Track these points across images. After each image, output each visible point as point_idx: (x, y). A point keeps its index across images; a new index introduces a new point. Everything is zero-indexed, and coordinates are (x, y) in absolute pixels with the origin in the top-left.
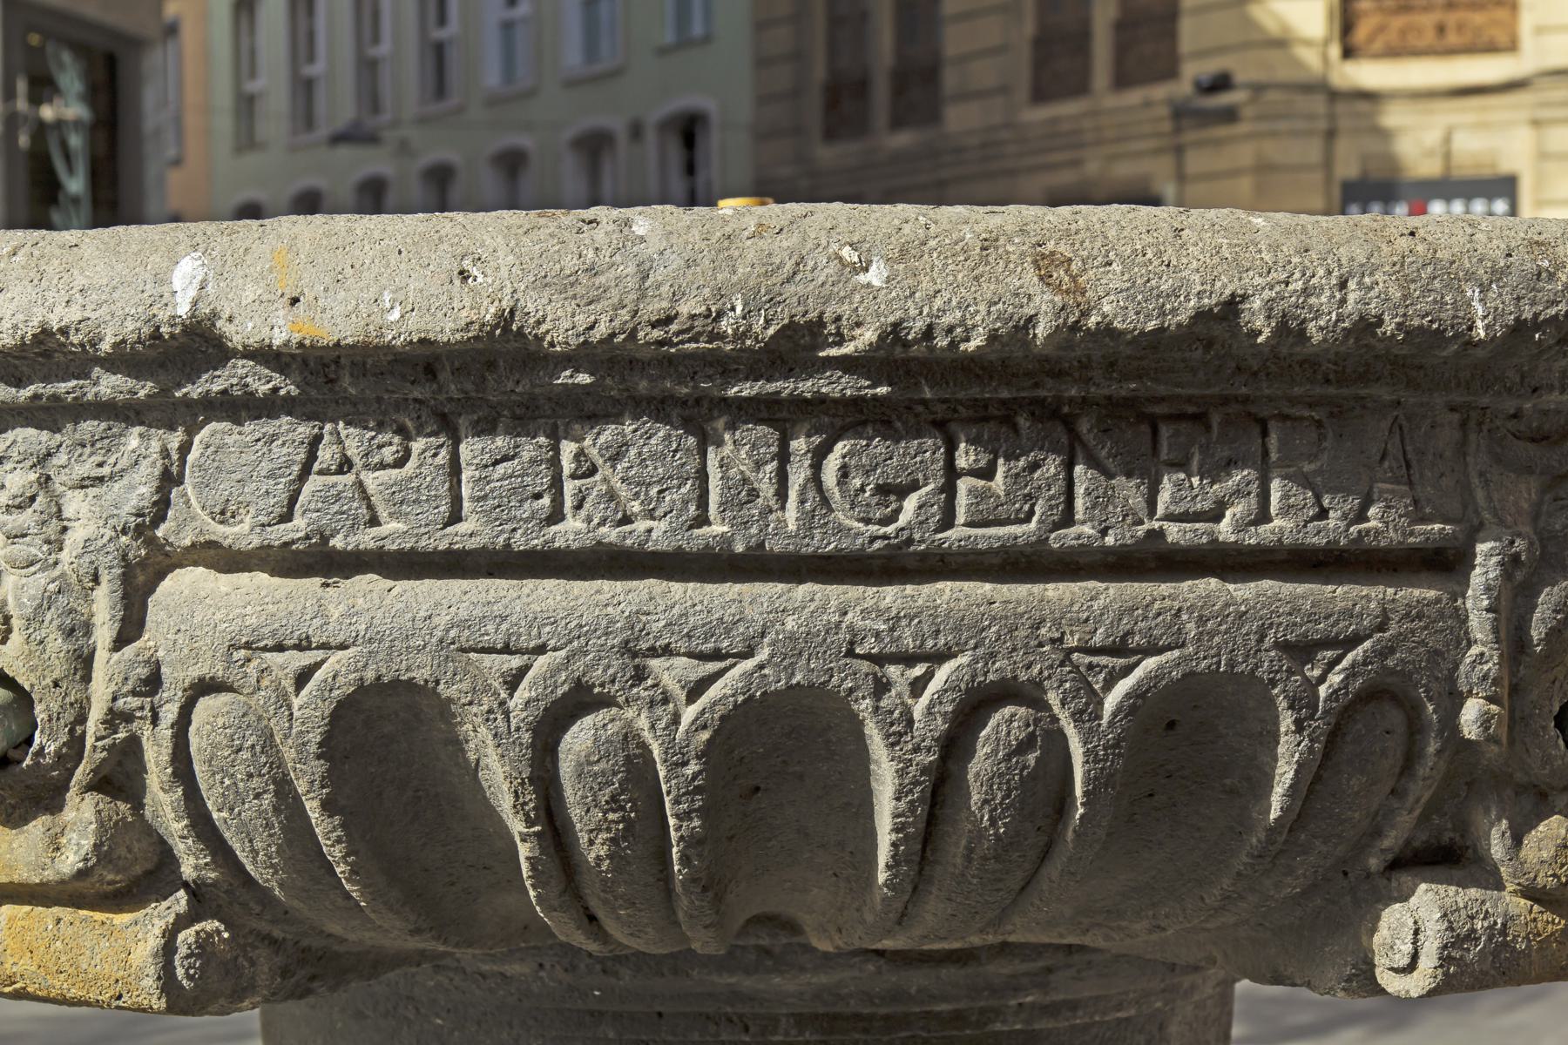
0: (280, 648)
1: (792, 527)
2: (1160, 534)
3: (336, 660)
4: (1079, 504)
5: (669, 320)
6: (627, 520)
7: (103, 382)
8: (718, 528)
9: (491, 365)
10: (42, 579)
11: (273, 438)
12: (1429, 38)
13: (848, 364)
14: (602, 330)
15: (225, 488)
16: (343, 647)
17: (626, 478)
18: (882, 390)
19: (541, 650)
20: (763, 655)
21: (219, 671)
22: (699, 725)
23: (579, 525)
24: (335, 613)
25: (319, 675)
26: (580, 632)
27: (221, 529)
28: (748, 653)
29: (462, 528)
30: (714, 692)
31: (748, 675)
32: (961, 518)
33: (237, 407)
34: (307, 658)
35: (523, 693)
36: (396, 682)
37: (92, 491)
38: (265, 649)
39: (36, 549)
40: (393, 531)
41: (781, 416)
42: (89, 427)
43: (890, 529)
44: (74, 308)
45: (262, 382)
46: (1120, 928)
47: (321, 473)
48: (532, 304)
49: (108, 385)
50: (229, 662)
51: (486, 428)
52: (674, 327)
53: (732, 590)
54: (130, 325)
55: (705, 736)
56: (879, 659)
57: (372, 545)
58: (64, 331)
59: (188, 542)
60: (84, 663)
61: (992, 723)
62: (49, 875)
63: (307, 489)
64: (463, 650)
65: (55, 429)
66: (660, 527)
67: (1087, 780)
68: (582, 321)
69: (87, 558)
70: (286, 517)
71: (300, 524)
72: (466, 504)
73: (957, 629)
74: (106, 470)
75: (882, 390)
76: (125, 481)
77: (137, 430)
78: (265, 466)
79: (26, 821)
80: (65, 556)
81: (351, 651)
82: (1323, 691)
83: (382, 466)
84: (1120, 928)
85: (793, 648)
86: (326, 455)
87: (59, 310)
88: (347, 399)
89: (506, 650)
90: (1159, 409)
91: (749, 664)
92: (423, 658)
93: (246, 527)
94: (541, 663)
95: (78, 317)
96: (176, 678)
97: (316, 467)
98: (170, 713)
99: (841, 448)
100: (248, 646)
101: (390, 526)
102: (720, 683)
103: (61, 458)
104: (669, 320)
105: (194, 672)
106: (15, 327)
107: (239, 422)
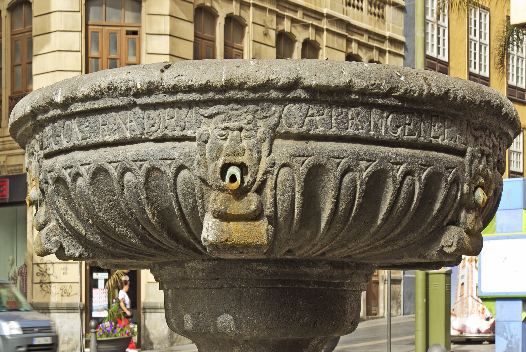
0: (299, 156)
1: (383, 133)
2: (431, 141)
3: (309, 159)
4: (422, 133)
5: (374, 84)
6: (358, 130)
7: (273, 93)
8: (372, 133)
9: (342, 93)
10: (254, 140)
11: (302, 108)
12: (18, 61)
13: (396, 97)
14: (364, 86)
15: (291, 119)
16: (311, 156)
17: (354, 121)
18: (400, 104)
19: (343, 158)
20: (377, 161)
21: (288, 161)
22: (367, 176)
23: (351, 130)
24: (309, 148)
25: (306, 162)
26: (350, 154)
27: (289, 129)
28: (375, 161)
29: (332, 130)
30: (369, 169)
31: (375, 165)
32: (406, 134)
33: (296, 100)
34: (304, 159)
35: (340, 167)
36: (319, 164)
37: (264, 120)
38: (297, 156)
39: (253, 133)
40: (320, 130)
41: (383, 108)
42: (265, 105)
43: (396, 135)
44: (274, 75)
45: (303, 95)
46: (396, 244)
47: (310, 116)
48: (355, 79)
49: (274, 94)
50: (290, 159)
51: (337, 107)
52: (374, 86)
53: (373, 147)
54: (286, 79)
55: (367, 179)
56: (393, 163)
57: (318, 133)
58: (272, 80)
59: (283, 132)
60: (259, 159)
61: (407, 179)
62: (249, 211)
63: (307, 120)
64: (331, 157)
65: (257, 105)
66: (364, 131)
67: (418, 194)
68: (362, 83)
69: (264, 135)
70: (302, 126)
71: (305, 128)
72: (333, 125)
73: (405, 158)
74: (268, 115)
75: (400, 104)
76: (272, 117)
77: (275, 106)
78: (300, 115)
79: (242, 199)
80: (258, 135)
81: (313, 157)
82: (449, 179)
83: (320, 115)
84: (396, 244)
85: (382, 159)
86: (310, 112)
87: (271, 75)
88: (318, 100)
89: (338, 158)
90: (433, 114)
91: (375, 163)
92: (325, 159)
93: (295, 128)
94: (344, 161)
95: (275, 77)
96: (279, 163)
97: (309, 115)
98: (276, 172)
99: (391, 116)
100: (293, 156)
101: (320, 129)
102: (370, 167)
103: (259, 112)
104: (374, 84)
105: (282, 162)
106: (263, 79)
107: (294, 104)
